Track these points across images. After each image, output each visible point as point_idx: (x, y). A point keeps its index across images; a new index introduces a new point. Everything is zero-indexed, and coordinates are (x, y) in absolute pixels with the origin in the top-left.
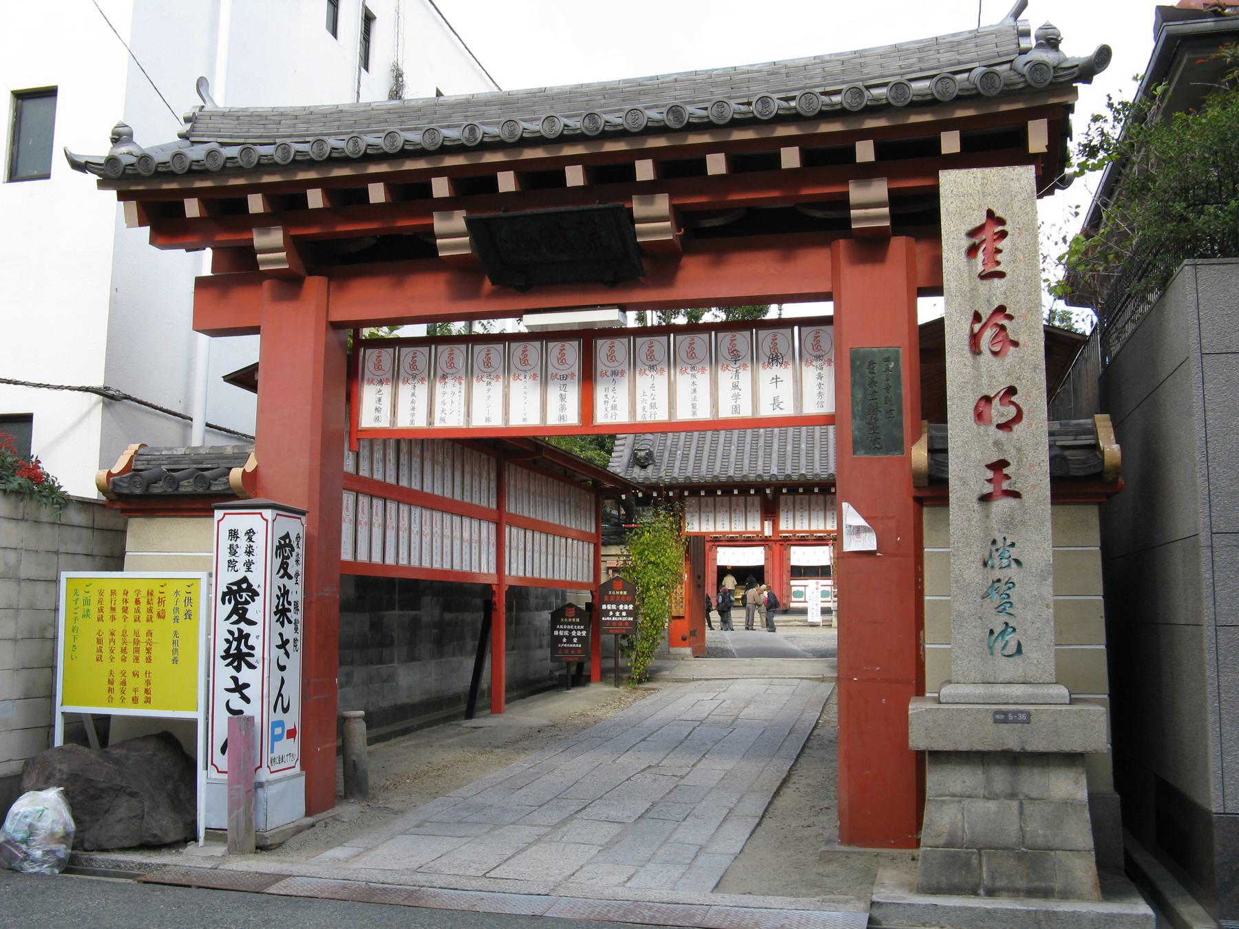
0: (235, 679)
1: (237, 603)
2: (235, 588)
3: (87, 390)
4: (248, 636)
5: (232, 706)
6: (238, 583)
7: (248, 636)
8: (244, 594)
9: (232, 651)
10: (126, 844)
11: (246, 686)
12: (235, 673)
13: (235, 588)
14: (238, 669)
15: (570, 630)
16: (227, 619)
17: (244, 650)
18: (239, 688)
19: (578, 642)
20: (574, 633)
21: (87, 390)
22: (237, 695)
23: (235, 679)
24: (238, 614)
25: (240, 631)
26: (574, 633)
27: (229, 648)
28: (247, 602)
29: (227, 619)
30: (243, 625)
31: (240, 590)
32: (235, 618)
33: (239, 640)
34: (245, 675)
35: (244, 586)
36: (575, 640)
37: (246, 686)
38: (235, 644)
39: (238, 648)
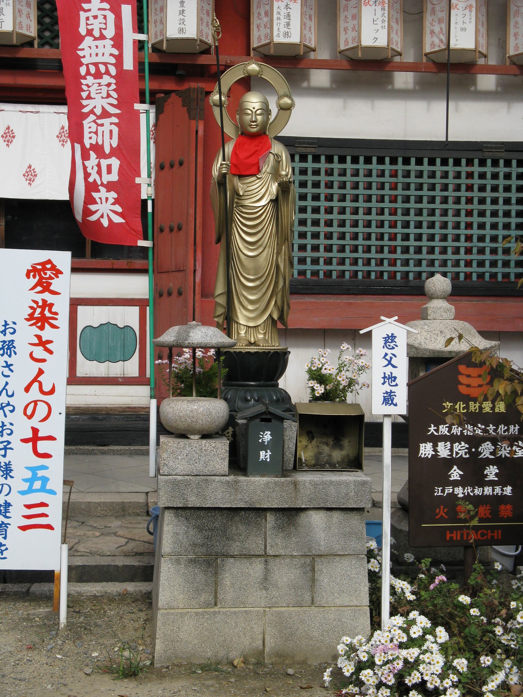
0: (39, 337)
1: (41, 278)
2: (39, 267)
3: (103, 141)
4: (51, 305)
5: (4, 373)
6: (43, 264)
7: (51, 305)
8: (49, 273)
9: (36, 315)
10: (510, 73)
11: (12, 365)
12: (39, 332)
13: (39, 267)
14: (42, 328)
15: (474, 442)
16: (32, 289)
17: (47, 314)
18: (42, 343)
19: (502, 482)
20: (486, 449)
21: (103, 141)
22: (7, 369)
23: (39, 337)
24: (42, 286)
25: (44, 301)
26: (486, 449)
27: (33, 313)
28: (51, 278)
29: (32, 289)
30: (47, 296)
31: (44, 269)
32: (39, 289)
33: (43, 308)
34: (47, 333)
35: (49, 266)
36: (492, 472)
37: (12, 365)
38: (39, 310)
39: (42, 313)
